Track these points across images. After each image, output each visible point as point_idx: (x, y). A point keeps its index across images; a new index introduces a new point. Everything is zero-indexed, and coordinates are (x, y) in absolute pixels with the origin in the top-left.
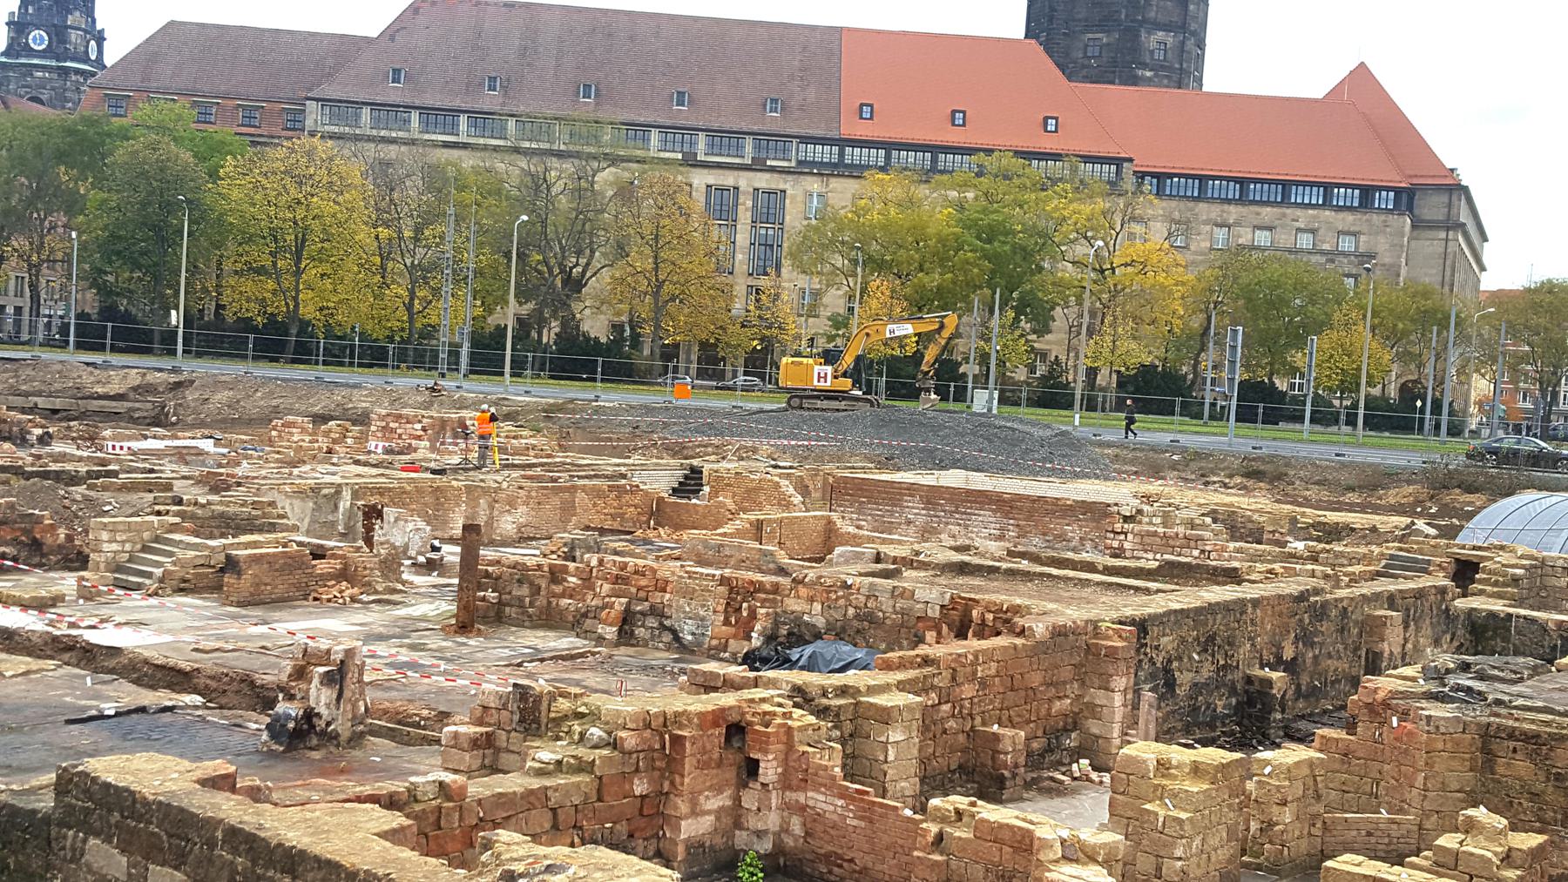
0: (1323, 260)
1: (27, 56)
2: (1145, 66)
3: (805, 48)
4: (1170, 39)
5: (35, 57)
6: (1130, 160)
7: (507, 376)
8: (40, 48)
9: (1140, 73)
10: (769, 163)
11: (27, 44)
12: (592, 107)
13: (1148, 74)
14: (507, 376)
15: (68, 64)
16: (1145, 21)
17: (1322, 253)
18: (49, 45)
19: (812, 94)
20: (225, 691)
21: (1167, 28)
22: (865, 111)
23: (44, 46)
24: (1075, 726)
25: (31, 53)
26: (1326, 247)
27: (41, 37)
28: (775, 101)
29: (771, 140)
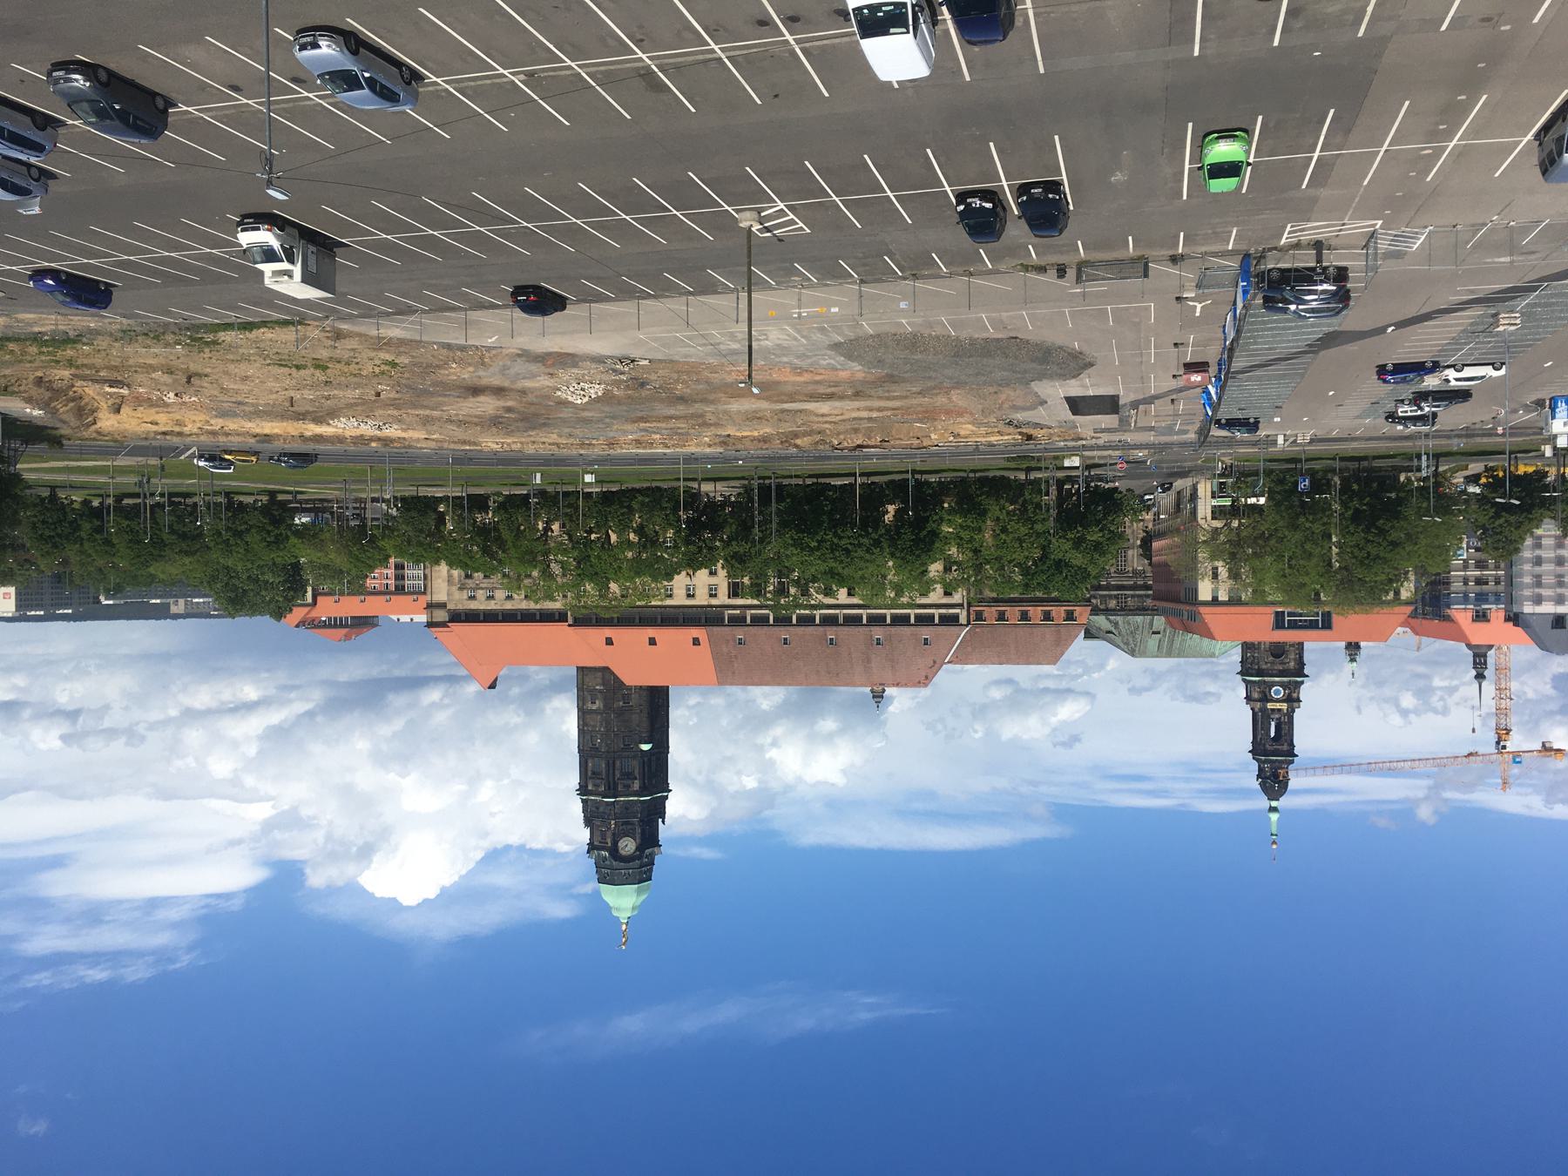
0: (482, 585)
1: (1284, 682)
2: (600, 691)
3: (734, 673)
4: (590, 706)
5: (1278, 682)
6: (569, 625)
7: (1215, 502)
8: (1275, 688)
9: (602, 688)
10: (738, 612)
11: (1285, 690)
12: (828, 633)
13: (598, 687)
14: (1215, 502)
15: (1257, 679)
16: (601, 714)
17: (482, 589)
18: (1270, 690)
19: (725, 649)
20: (99, 350)
21: (592, 712)
22: (696, 642)
23: (1274, 689)
24: (40, 353)
25: (1282, 684)
26: (481, 592)
27: (1278, 690)
28: (740, 643)
29: (738, 621)
